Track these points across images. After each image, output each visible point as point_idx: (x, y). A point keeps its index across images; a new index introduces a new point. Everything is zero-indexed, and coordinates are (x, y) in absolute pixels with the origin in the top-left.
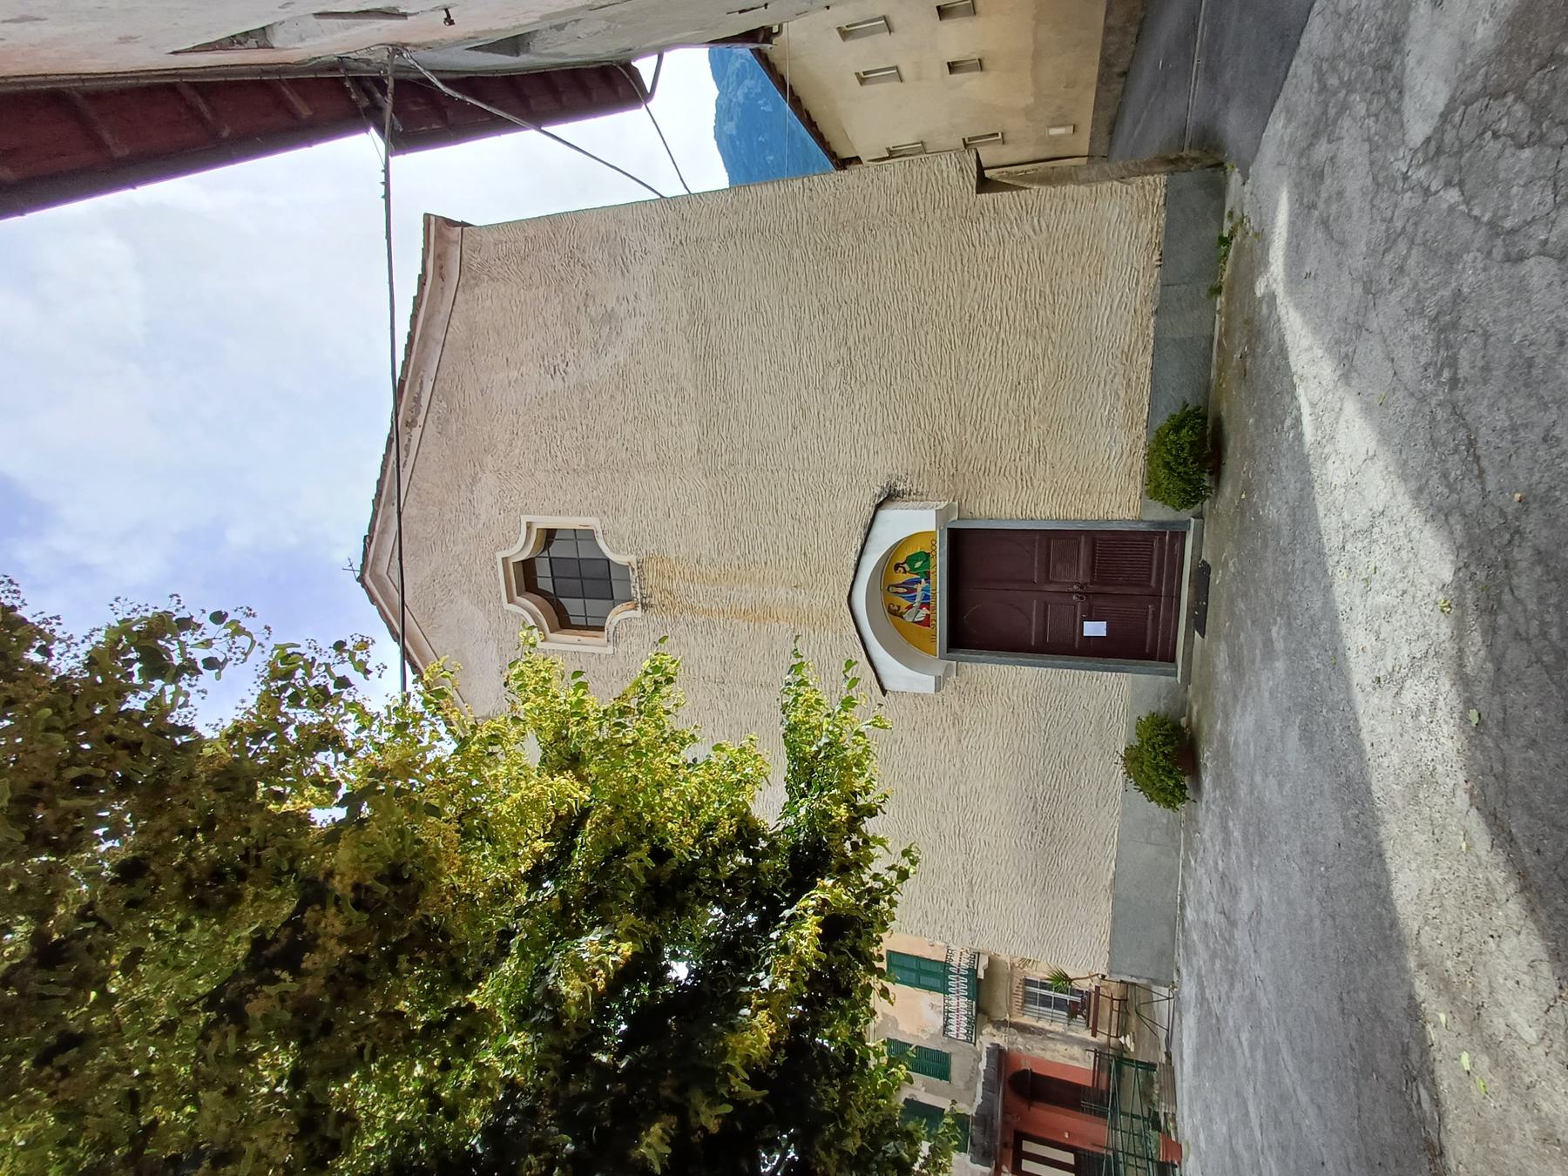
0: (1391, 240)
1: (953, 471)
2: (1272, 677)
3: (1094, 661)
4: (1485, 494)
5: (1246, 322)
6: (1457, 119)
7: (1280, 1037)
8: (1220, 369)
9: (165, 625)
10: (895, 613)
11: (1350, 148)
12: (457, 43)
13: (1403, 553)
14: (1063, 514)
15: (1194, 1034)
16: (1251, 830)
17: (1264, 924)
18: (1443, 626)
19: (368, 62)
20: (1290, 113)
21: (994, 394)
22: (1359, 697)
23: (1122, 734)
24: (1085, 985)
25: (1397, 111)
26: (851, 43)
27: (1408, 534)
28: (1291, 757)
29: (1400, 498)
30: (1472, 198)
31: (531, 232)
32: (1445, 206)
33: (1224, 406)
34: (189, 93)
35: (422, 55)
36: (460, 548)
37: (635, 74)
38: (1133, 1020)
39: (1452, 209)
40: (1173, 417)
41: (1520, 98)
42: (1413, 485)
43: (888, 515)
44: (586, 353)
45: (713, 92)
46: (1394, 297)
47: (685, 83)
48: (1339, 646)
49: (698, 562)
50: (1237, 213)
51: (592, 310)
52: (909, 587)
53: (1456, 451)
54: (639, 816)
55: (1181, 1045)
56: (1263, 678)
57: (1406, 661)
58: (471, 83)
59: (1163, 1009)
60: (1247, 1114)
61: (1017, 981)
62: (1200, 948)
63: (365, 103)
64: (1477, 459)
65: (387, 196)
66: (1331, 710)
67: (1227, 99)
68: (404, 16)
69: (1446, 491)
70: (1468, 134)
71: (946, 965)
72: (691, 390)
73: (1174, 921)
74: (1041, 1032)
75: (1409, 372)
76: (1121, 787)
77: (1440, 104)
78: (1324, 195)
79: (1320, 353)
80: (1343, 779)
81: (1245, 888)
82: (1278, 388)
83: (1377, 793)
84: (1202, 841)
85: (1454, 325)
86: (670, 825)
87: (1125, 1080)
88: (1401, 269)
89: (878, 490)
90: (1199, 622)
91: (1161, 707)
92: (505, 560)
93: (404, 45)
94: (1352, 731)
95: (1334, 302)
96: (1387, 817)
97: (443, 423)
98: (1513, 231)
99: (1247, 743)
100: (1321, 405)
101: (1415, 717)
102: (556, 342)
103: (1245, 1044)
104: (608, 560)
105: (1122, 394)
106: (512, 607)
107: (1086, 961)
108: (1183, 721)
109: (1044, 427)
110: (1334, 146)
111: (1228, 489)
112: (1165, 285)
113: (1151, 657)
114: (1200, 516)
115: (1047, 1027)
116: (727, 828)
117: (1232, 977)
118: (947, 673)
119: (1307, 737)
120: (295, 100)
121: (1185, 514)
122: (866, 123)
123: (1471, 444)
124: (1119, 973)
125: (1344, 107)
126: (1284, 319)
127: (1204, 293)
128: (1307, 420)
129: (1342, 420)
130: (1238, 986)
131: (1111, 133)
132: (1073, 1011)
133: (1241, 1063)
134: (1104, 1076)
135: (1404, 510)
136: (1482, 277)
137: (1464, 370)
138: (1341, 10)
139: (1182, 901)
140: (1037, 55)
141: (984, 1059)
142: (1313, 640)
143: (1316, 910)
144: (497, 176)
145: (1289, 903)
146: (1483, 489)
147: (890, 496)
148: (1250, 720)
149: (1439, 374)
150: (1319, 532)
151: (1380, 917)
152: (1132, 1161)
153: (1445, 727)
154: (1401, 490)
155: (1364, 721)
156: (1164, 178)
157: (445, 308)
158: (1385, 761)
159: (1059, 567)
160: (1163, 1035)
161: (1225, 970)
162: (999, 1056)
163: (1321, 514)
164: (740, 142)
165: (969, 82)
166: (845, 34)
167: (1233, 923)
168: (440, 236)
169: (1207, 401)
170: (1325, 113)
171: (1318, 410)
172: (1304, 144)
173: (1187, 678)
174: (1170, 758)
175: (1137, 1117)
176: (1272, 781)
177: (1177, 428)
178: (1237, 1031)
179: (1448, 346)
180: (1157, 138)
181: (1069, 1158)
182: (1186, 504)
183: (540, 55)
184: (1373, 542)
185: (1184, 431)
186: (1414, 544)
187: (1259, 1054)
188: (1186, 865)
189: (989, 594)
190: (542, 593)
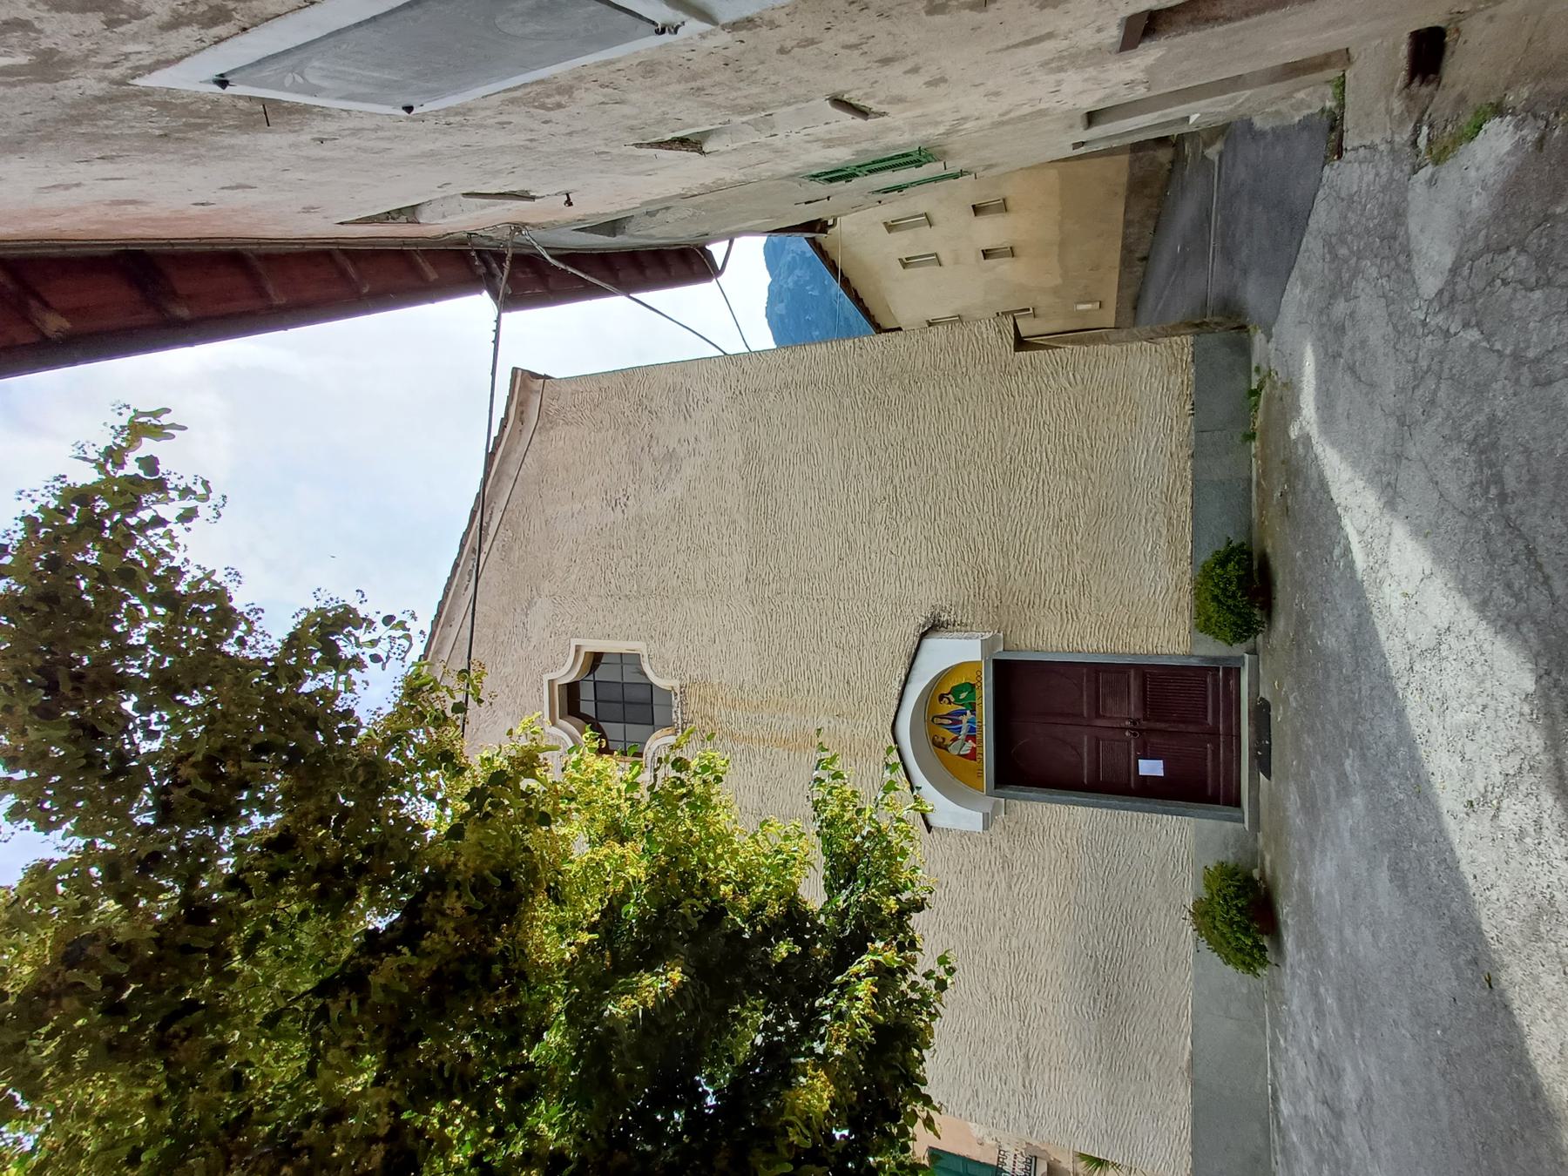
0: (1419, 378)
1: (997, 603)
2: (1351, 814)
3: (1153, 803)
4: (1554, 599)
6: (1466, 272)
8: (1261, 508)
9: (346, 619)
10: (940, 745)
11: (1367, 302)
12: (568, 224)
13: (1477, 666)
16: (1348, 995)
18: (1534, 737)
19: (491, 239)
21: (1036, 530)
22: (1451, 824)
23: (1189, 886)
25: (1408, 271)
27: (1479, 648)
28: (1383, 902)
29: (1464, 612)
30: (1492, 335)
31: (605, 384)
32: (1466, 344)
33: (1269, 544)
34: (341, 259)
35: (537, 234)
36: (509, 670)
37: (709, 255)
39: (1473, 346)
40: (1217, 552)
41: (1523, 250)
42: (1477, 598)
43: (930, 643)
45: (767, 279)
46: (1429, 428)
47: (746, 265)
48: (1422, 772)
49: (741, 688)
50: (1264, 366)
51: (655, 451)
52: (954, 718)
53: (1515, 561)
56: (1341, 817)
57: (1499, 779)
58: (574, 258)
63: (482, 270)
64: (1539, 566)
65: (496, 342)
66: (1423, 842)
67: (1245, 272)
68: (533, 198)
69: (1512, 600)
70: (1478, 284)
73: (1265, 1114)
75: (1455, 492)
76: (1191, 948)
77: (1448, 260)
78: (1348, 345)
79: (1360, 484)
81: (1349, 1069)
82: (1322, 521)
83: (1490, 932)
85: (1494, 446)
86: (722, 887)
88: (1432, 402)
89: (922, 620)
90: (1263, 763)
91: (1230, 857)
92: (551, 682)
94: (1450, 865)
95: (1370, 437)
96: (1506, 959)
97: (507, 550)
98: (1537, 360)
99: (1330, 892)
100: (1369, 533)
101: (1520, 838)
104: (651, 685)
106: (554, 730)
108: (1256, 874)
110: (1353, 303)
111: (1281, 623)
112: (1200, 432)
113: (1214, 800)
114: (1253, 652)
116: (774, 909)
119: (1400, 878)
121: (1238, 649)
122: (908, 298)
123: (1531, 552)
125: (1356, 272)
126: (1322, 456)
127: (1238, 439)
128: (1356, 548)
129: (1392, 544)
131: (1135, 308)
135: (1471, 624)
136: (1514, 401)
137: (1511, 484)
138: (1343, 195)
140: (1063, 244)
142: (1391, 769)
145: (1405, 1082)
146: (1552, 595)
147: (934, 627)
149: (1487, 491)
150: (1383, 656)
151: (1519, 1084)
153: (1556, 847)
154: (1464, 604)
155: (1461, 851)
157: (521, 449)
158: (1493, 894)
159: (1110, 702)
163: (1383, 637)
164: (790, 316)
165: (1003, 266)
167: (1338, 1115)
168: (524, 386)
171: (1367, 537)
174: (1245, 914)
176: (1366, 934)
179: (1491, 465)
180: (1182, 308)
182: (1238, 638)
184: (1441, 659)
185: (1230, 566)
186: (1487, 657)
188: (1274, 1045)
189: (1040, 729)
190: (585, 718)
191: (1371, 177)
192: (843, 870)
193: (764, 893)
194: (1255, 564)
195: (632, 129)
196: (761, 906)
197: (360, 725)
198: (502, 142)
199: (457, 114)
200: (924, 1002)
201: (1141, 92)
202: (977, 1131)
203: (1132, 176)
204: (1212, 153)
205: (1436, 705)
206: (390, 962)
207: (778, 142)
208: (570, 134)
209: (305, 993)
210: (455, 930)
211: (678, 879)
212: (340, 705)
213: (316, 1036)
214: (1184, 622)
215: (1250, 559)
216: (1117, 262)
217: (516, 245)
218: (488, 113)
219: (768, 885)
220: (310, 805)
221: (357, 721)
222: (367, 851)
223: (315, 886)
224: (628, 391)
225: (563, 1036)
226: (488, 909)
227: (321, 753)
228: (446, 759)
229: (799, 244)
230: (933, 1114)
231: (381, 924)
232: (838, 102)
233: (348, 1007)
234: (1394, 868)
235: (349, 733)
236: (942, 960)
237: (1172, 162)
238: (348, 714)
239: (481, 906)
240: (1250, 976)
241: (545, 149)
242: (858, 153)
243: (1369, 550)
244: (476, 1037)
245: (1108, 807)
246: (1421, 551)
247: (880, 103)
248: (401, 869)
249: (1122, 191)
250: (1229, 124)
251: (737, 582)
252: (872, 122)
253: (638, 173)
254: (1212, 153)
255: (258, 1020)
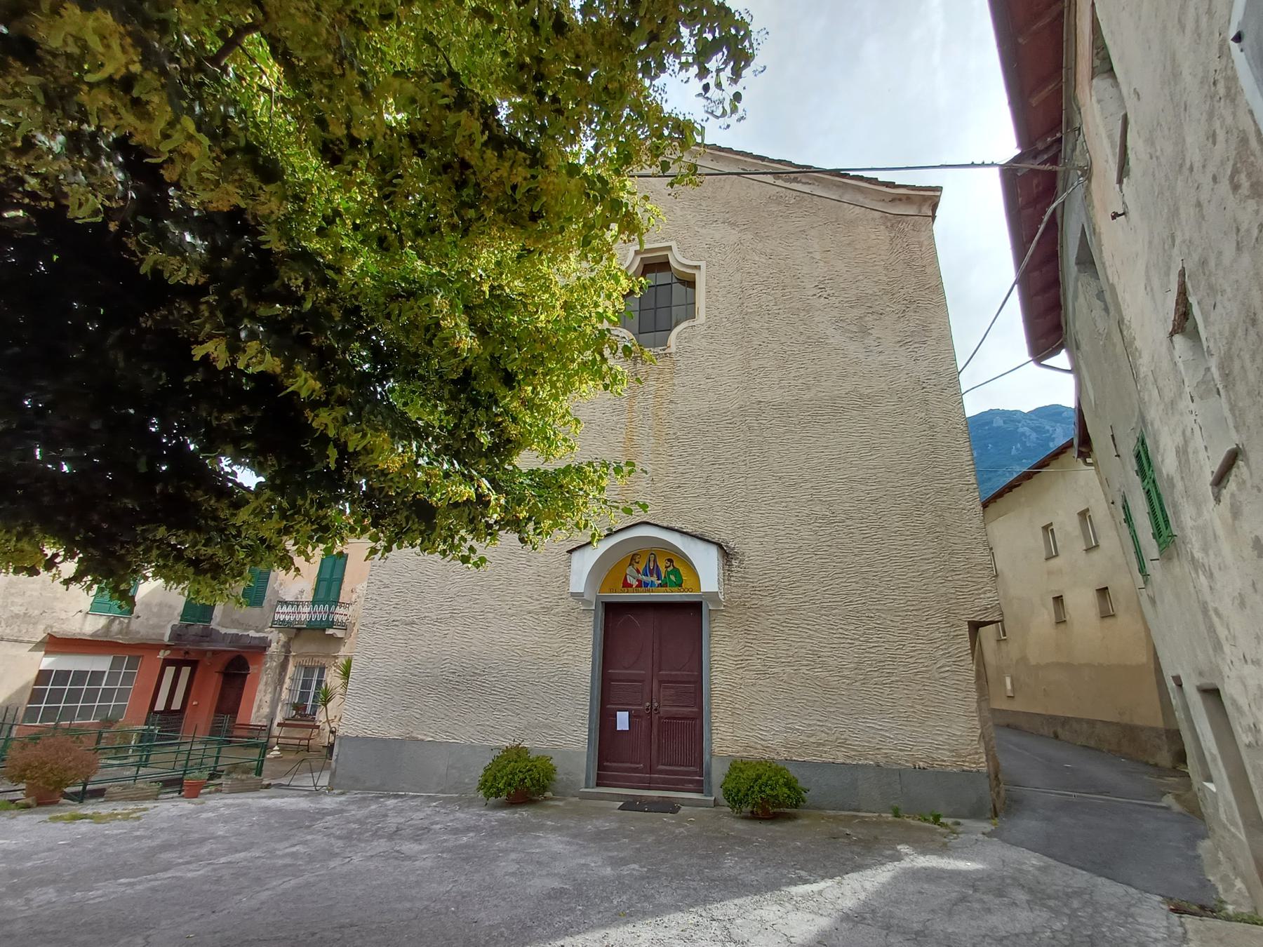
2: (597, 865)
5: (876, 838)
7: (308, 877)
8: (835, 817)
10: (633, 559)
12: (1090, 219)
14: (716, 693)
15: (293, 807)
17: (396, 862)
19: (1074, 150)
20: (1044, 869)
21: (810, 637)
24: (321, 717)
26: (1076, 519)
28: (537, 882)
31: (929, 270)
33: (806, 822)
35: (1079, 192)
36: (679, 213)
38: (292, 756)
43: (713, 552)
44: (836, 313)
45: (1026, 409)
47: (1051, 386)
50: (960, 829)
51: (869, 318)
54: (542, 363)
55: (283, 797)
56: (595, 859)
58: (1054, 227)
59: (307, 781)
60: (237, 851)
61: (323, 661)
62: (365, 812)
65: (973, 165)
66: (583, 913)
68: (1120, 182)
71: (336, 602)
72: (807, 397)
73: (385, 790)
74: (281, 682)
78: (985, 898)
79: (863, 896)
80: (529, 924)
81: (422, 847)
84: (453, 811)
86: (530, 388)
87: (242, 750)
89: (731, 545)
90: (630, 805)
91: (559, 776)
93: (1089, 179)
97: (778, 200)
99: (540, 846)
100: (821, 899)
102: (844, 289)
103: (294, 849)
104: (670, 330)
105: (812, 740)
106: (632, 254)
107: (347, 715)
108: (548, 794)
109: (785, 677)
110: (1026, 906)
111: (741, 826)
112: (900, 773)
113: (601, 767)
115: (285, 686)
116: (513, 431)
117: (348, 837)
118: (589, 602)
119: (557, 894)
120: (1044, 93)
121: (718, 793)
122: (1014, 534)
124: (340, 744)
125: (1056, 913)
129: (813, 916)
130: (340, 843)
131: (1008, 726)
132: (299, 707)
133: (278, 846)
134: (244, 733)
139: (401, 796)
141: (257, 635)
143: (418, 904)
144: (976, 243)
147: (726, 554)
148: (559, 848)
152: (183, 757)
156: (985, 770)
160: (284, 781)
161: (352, 832)
162: (261, 648)
163: (736, 901)
164: (993, 431)
165: (1046, 614)
166: (1084, 515)
168: (925, 199)
169: (808, 808)
170: (1049, 898)
172: (1022, 881)
173: (585, 797)
174: (519, 785)
175: (216, 762)
176: (513, 868)
177: (788, 784)
178: (305, 843)
181: (176, 705)
182: (727, 793)
183: (1077, 280)
185: (786, 790)
187: (288, 861)
189: (649, 634)
191: (1154, 935)
192: (547, 483)
193: (525, 423)
194: (788, 810)
195: (1204, 263)
196: (515, 420)
197: (652, 79)
198: (1189, 140)
199: (1228, 89)
200: (453, 547)
201: (1244, 738)
202: (362, 588)
203: (1142, 729)
204: (1168, 800)
205: (686, 934)
206: (477, 126)
207: (1185, 403)
208: (1199, 204)
209: (449, 63)
210: (501, 177)
211: (546, 352)
212: (670, 60)
213: (420, 75)
214: (736, 751)
215: (791, 806)
216: (1051, 712)
217: (1067, 173)
218: (1229, 120)
219: (531, 425)
220: (590, 46)
221: (656, 76)
222: (555, 99)
223: (528, 60)
224: (919, 294)
225: (422, 272)
226: (515, 202)
227: (631, 49)
228: (626, 158)
229: (1063, 434)
230: (379, 554)
231: (503, 114)
232: (1233, 458)
233: (445, 96)
234: (562, 892)
235: (646, 70)
236: (483, 560)
237: (1156, 765)
238: (662, 68)
239: (518, 196)
240: (477, 785)
241: (1180, 183)
242: (1170, 480)
243: (806, 897)
244: (420, 204)
245: (592, 687)
246: (809, 937)
247: (1233, 495)
248: (542, 129)
249: (1126, 719)
250: (1201, 817)
251: (757, 394)
252: (1209, 490)
253: (1148, 278)
254: (1168, 800)
255: (429, 29)
